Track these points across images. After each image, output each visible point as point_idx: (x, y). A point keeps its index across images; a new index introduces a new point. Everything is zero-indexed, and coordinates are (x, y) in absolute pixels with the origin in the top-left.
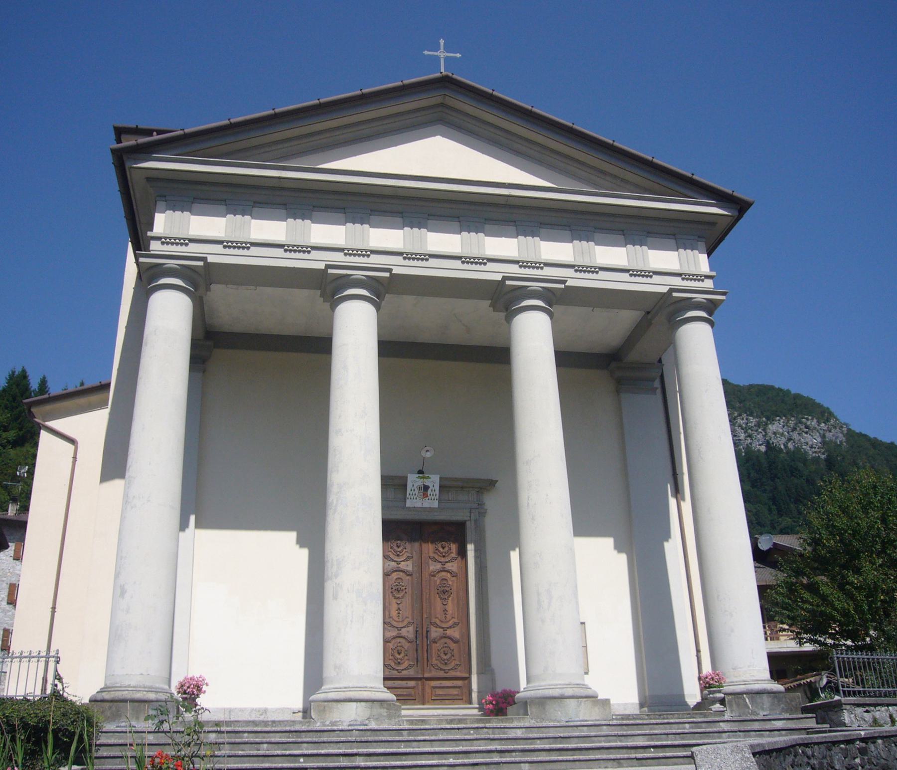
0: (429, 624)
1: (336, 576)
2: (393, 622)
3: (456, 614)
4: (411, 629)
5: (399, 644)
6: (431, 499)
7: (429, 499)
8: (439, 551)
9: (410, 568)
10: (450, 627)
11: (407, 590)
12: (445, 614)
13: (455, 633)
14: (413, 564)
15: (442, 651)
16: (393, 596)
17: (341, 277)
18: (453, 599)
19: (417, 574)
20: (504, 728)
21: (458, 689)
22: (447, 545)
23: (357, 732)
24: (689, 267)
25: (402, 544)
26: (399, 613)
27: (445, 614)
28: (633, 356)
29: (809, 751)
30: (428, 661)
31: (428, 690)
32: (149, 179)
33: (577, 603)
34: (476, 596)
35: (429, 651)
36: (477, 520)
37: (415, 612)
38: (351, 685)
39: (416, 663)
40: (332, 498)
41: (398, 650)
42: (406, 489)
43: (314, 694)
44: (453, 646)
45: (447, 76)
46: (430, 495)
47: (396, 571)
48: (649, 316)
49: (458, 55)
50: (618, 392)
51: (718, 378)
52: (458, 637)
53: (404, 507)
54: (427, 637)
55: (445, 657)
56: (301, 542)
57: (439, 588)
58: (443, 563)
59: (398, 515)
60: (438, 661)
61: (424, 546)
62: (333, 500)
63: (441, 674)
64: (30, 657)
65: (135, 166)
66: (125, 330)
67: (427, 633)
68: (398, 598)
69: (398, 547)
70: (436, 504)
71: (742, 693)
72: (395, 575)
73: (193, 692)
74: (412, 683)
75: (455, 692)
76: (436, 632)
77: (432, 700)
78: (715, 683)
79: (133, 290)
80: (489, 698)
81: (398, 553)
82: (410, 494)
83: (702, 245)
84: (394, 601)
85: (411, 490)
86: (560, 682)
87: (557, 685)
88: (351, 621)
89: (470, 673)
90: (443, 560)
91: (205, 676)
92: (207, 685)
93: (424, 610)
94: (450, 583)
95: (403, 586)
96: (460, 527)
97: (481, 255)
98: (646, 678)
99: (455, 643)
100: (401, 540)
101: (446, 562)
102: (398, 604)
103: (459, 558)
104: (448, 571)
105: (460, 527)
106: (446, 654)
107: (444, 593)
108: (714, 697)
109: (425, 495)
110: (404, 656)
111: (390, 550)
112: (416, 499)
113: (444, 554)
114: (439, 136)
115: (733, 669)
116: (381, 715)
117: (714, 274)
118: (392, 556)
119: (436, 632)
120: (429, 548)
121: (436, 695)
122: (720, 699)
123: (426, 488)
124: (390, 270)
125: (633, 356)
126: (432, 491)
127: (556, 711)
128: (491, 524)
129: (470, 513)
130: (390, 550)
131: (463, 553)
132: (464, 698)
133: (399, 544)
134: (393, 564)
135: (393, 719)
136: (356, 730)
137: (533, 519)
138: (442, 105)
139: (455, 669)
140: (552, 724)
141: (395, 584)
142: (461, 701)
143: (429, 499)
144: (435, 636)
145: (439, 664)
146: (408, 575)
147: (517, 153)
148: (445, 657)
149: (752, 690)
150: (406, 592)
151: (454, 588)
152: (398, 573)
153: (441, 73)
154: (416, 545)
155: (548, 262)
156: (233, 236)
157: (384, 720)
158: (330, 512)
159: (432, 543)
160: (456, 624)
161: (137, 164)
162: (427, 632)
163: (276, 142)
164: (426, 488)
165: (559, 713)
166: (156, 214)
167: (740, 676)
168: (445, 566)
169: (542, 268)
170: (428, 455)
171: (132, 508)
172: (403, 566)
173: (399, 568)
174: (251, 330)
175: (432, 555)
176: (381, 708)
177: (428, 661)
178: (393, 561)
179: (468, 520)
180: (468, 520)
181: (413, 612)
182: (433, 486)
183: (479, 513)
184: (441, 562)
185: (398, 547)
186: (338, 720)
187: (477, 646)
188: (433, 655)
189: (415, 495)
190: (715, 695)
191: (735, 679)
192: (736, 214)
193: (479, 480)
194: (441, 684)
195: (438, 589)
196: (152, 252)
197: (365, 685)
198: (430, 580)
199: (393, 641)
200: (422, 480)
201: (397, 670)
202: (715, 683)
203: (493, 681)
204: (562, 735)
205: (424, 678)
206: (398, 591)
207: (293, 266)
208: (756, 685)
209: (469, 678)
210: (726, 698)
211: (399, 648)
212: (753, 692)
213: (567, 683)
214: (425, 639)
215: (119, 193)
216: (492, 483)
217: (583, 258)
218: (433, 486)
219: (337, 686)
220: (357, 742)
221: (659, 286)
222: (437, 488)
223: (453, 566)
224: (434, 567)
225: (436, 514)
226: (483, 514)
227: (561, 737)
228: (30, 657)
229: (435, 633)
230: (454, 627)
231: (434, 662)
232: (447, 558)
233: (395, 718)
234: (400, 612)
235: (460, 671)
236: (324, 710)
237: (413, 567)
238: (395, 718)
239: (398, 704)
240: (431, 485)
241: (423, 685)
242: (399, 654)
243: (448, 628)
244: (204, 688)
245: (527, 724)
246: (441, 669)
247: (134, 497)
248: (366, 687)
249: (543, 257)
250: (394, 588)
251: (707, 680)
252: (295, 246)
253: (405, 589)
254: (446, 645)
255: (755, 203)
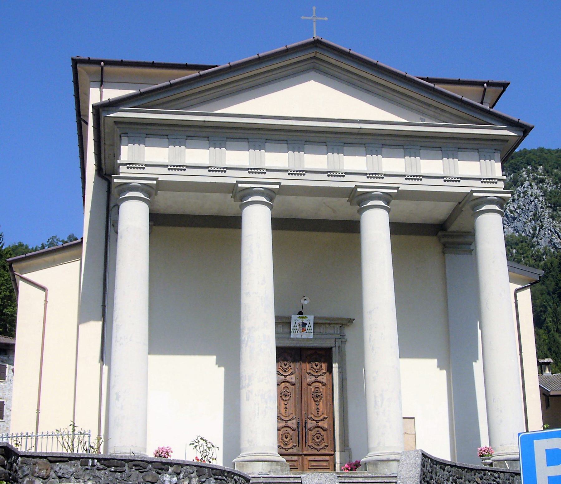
0: (307, 418)
1: (248, 385)
2: (282, 416)
3: (325, 411)
4: (294, 421)
5: (286, 432)
6: (308, 332)
7: (306, 332)
8: (314, 368)
9: (293, 380)
10: (321, 420)
11: (291, 395)
12: (318, 411)
13: (325, 424)
14: (295, 377)
15: (315, 436)
16: (282, 399)
17: (245, 189)
18: (323, 402)
19: (299, 384)
20: (351, 477)
21: (326, 462)
22: (319, 364)
23: (263, 478)
24: (487, 174)
25: (288, 363)
26: (286, 411)
27: (318, 411)
28: (454, 227)
29: (496, 475)
30: (306, 443)
31: (306, 462)
32: (115, 122)
33: (400, 403)
34: (339, 399)
35: (307, 436)
36: (340, 346)
37: (297, 410)
38: (258, 452)
39: (297, 445)
40: (244, 336)
41: (285, 436)
42: (291, 325)
43: (236, 458)
44: (323, 433)
45: (318, 40)
46: (307, 329)
47: (284, 382)
48: (461, 205)
49: (326, 19)
50: (444, 253)
51: (502, 253)
52: (326, 427)
53: (289, 338)
54: (305, 427)
55: (317, 441)
56: (219, 363)
57: (314, 394)
58: (316, 377)
59: (286, 343)
60: (312, 443)
61: (303, 365)
62: (245, 338)
63: (315, 452)
64: (48, 435)
65: (108, 116)
66: (89, 213)
67: (305, 425)
68: (285, 400)
69: (285, 365)
70: (311, 336)
71: (504, 460)
72: (283, 385)
73: (165, 456)
74: (295, 458)
75: (325, 464)
76: (311, 423)
77: (309, 469)
78: (486, 453)
79: (93, 184)
80: (346, 465)
81: (285, 370)
82: (293, 329)
83: (498, 156)
84: (283, 402)
85: (294, 326)
86: (388, 452)
87: (385, 453)
88: (258, 414)
89: (335, 451)
90: (316, 374)
91: (171, 446)
92: (172, 452)
93: (303, 409)
94: (321, 390)
95: (289, 392)
96: (329, 351)
97: (341, 170)
98: (456, 455)
99: (324, 431)
100: (287, 361)
101: (318, 376)
102: (285, 404)
103: (328, 373)
104: (319, 382)
105: (329, 351)
106: (318, 439)
107: (317, 397)
108: (485, 462)
109: (304, 330)
110: (290, 440)
111: (280, 367)
112: (298, 332)
113: (317, 370)
114: (312, 81)
115: (501, 446)
116: (277, 469)
117: (505, 177)
118: (281, 372)
119: (311, 423)
120: (307, 367)
121: (312, 466)
122: (490, 463)
123: (305, 324)
124: (279, 184)
125: (454, 227)
126: (308, 326)
127: (384, 468)
128: (349, 349)
129: (335, 341)
130: (280, 367)
131: (330, 370)
132: (330, 468)
133: (286, 364)
134: (282, 377)
135: (284, 472)
136: (262, 477)
137: (373, 349)
138: (315, 58)
139: (325, 448)
140: (380, 475)
141: (283, 391)
142: (328, 470)
143: (306, 332)
144: (311, 426)
145: (313, 445)
146: (292, 385)
147: (368, 91)
148: (317, 441)
149: (511, 458)
150: (291, 397)
151: (324, 394)
152: (285, 383)
153: (314, 38)
154: (298, 364)
155: (387, 173)
156: (174, 161)
157: (279, 472)
158: (243, 346)
159: (309, 362)
160: (325, 418)
161: (109, 115)
162: (305, 423)
163: (200, 92)
164: (305, 324)
165: (386, 470)
166: (122, 147)
167: (504, 450)
168: (317, 379)
169: (383, 178)
170: (306, 302)
171: (120, 345)
172: (288, 378)
173: (286, 380)
174: (180, 212)
175: (308, 371)
176: (277, 466)
177: (306, 443)
178: (282, 375)
179: (334, 347)
180: (334, 347)
181: (295, 409)
182: (309, 323)
183: (341, 341)
184: (315, 376)
185: (285, 365)
186: (251, 472)
187: (340, 430)
188: (310, 439)
189: (297, 329)
190: (486, 461)
191: (501, 452)
192: (522, 134)
193: (342, 319)
194: (314, 458)
195: (313, 395)
196: (121, 175)
197: (267, 452)
198: (307, 388)
199: (282, 430)
200: (302, 319)
201: (285, 449)
202: (486, 453)
203: (350, 456)
204: (386, 481)
205: (303, 454)
206: (285, 395)
207: (214, 182)
208: (514, 455)
209: (333, 454)
210: (493, 463)
211: (286, 434)
212: (511, 459)
213: (392, 452)
214: (304, 428)
215: (93, 127)
216: (351, 321)
217: (412, 170)
218: (309, 323)
219: (250, 453)
220: (264, 483)
221: (462, 188)
222: (312, 325)
223: (323, 379)
224: (310, 380)
225: (311, 342)
226: (344, 342)
227: (385, 482)
228: (48, 435)
229: (311, 424)
230: (324, 420)
231: (310, 443)
232: (319, 373)
233: (285, 472)
234: (287, 410)
235: (328, 450)
236: (243, 466)
237: (295, 379)
238: (285, 472)
239: (287, 463)
240: (308, 323)
241: (303, 459)
242: (286, 438)
243: (319, 421)
244: (170, 454)
245: (365, 475)
246: (315, 449)
247: (121, 338)
248: (268, 453)
249: (383, 170)
250: (283, 394)
251: (481, 451)
252: (216, 167)
253: (290, 394)
254: (318, 432)
255: (534, 128)
